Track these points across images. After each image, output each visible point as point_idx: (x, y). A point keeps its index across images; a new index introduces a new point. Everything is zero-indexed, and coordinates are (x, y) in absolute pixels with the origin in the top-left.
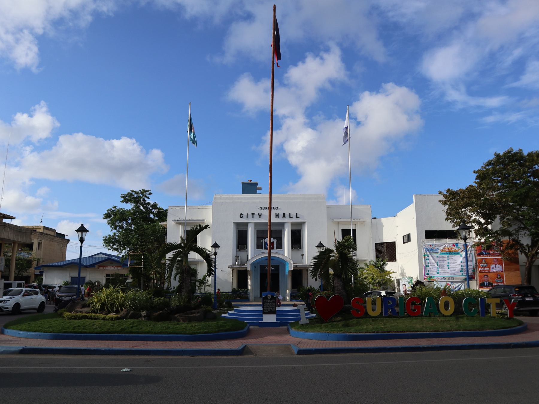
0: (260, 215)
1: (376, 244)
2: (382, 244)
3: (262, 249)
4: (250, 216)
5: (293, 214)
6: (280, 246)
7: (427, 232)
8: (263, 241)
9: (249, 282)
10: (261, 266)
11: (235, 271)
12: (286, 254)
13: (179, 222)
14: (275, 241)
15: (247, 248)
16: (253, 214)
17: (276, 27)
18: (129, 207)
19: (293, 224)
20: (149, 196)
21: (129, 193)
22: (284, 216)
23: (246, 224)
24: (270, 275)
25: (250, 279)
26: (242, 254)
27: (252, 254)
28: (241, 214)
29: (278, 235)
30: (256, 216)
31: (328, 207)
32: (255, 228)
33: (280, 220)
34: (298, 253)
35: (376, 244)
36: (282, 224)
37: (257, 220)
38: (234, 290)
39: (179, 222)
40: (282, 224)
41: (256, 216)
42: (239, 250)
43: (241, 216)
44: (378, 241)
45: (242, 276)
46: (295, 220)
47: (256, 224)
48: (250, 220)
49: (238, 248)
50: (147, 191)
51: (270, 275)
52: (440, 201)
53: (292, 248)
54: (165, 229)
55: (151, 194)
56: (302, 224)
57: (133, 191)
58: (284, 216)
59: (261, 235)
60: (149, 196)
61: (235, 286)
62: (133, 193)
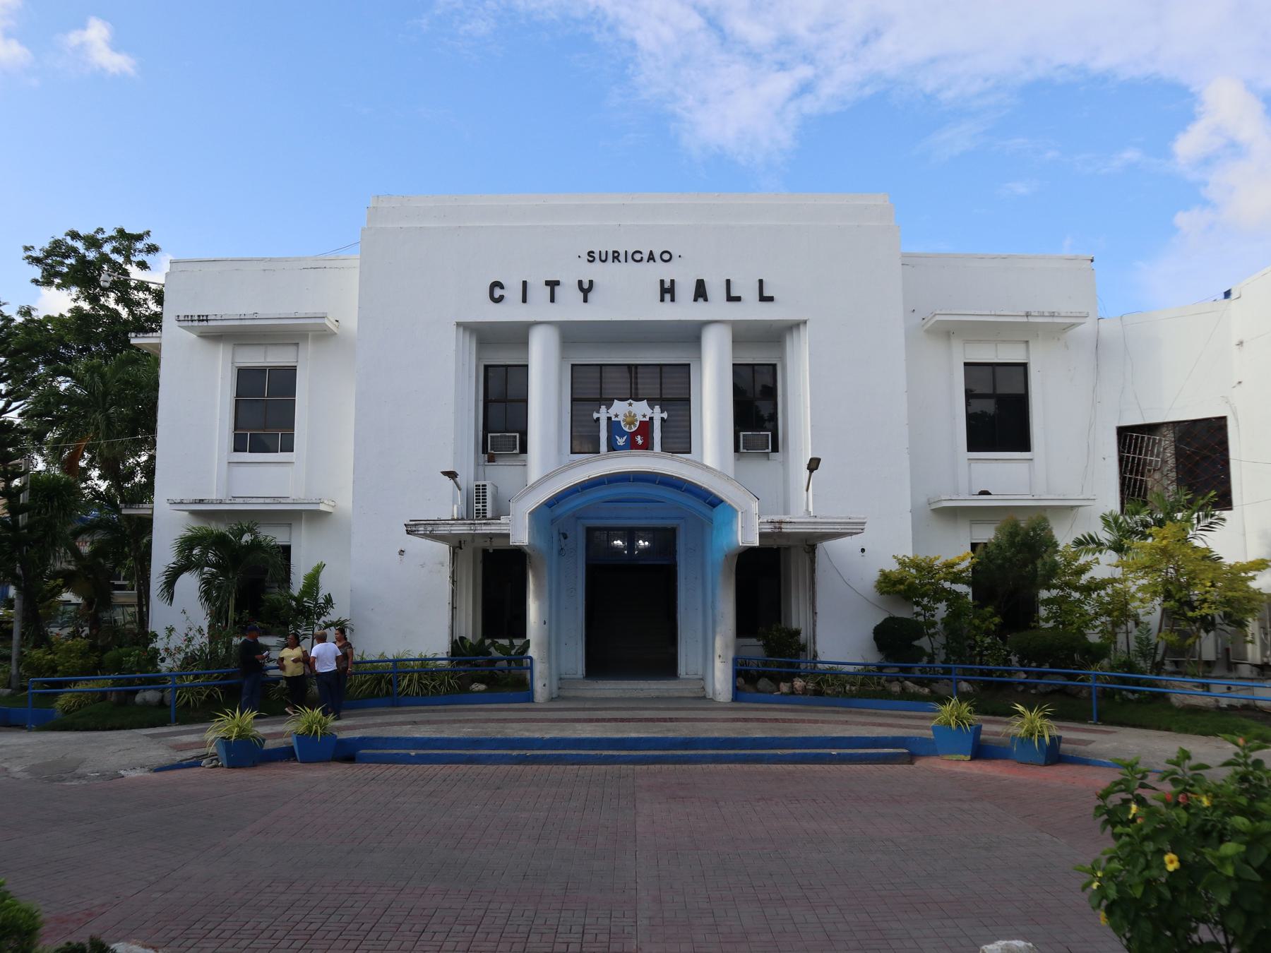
0: (586, 290)
1: (1125, 433)
2: (1151, 429)
3: (596, 451)
4: (539, 293)
5: (747, 290)
6: (679, 438)
7: (1216, 428)
8: (603, 414)
9: (534, 611)
10: (590, 531)
11: (466, 554)
12: (710, 458)
13: (218, 335)
14: (658, 414)
15: (524, 449)
16: (553, 284)
17: (851, 534)
18: (59, 302)
19: (743, 335)
20: (149, 259)
21: (57, 244)
22: (701, 291)
23: (518, 335)
24: (629, 583)
25: (538, 596)
26: (502, 475)
27: (549, 461)
28: (497, 284)
29: (673, 391)
30: (569, 293)
31: (908, 261)
32: (563, 357)
33: (684, 310)
34: (761, 469)
35: (1125, 433)
36: (691, 335)
37: (571, 309)
38: (458, 646)
39: (218, 335)
40: (691, 335)
41: (569, 293)
42: (491, 459)
43: (495, 291)
44: (1134, 419)
45: (497, 577)
46: (752, 311)
47: (570, 335)
48: (539, 309)
49: (485, 451)
50: (139, 238)
51: (629, 583)
52: (854, 529)
53: (737, 449)
54: (151, 360)
55: (152, 249)
56: (778, 335)
57: (74, 235)
58: (701, 291)
59: (588, 390)
60: (149, 259)
61: (469, 628)
62: (79, 245)
